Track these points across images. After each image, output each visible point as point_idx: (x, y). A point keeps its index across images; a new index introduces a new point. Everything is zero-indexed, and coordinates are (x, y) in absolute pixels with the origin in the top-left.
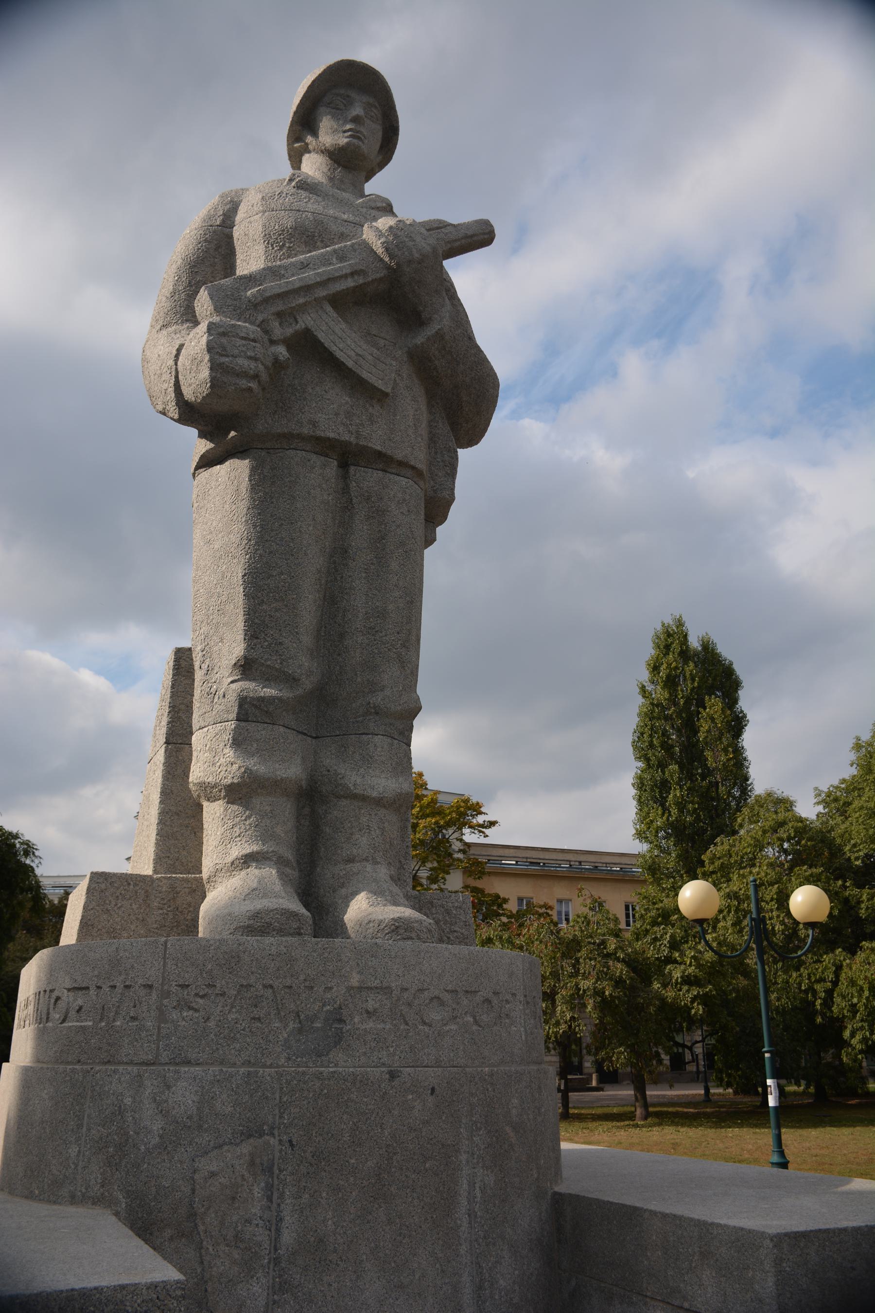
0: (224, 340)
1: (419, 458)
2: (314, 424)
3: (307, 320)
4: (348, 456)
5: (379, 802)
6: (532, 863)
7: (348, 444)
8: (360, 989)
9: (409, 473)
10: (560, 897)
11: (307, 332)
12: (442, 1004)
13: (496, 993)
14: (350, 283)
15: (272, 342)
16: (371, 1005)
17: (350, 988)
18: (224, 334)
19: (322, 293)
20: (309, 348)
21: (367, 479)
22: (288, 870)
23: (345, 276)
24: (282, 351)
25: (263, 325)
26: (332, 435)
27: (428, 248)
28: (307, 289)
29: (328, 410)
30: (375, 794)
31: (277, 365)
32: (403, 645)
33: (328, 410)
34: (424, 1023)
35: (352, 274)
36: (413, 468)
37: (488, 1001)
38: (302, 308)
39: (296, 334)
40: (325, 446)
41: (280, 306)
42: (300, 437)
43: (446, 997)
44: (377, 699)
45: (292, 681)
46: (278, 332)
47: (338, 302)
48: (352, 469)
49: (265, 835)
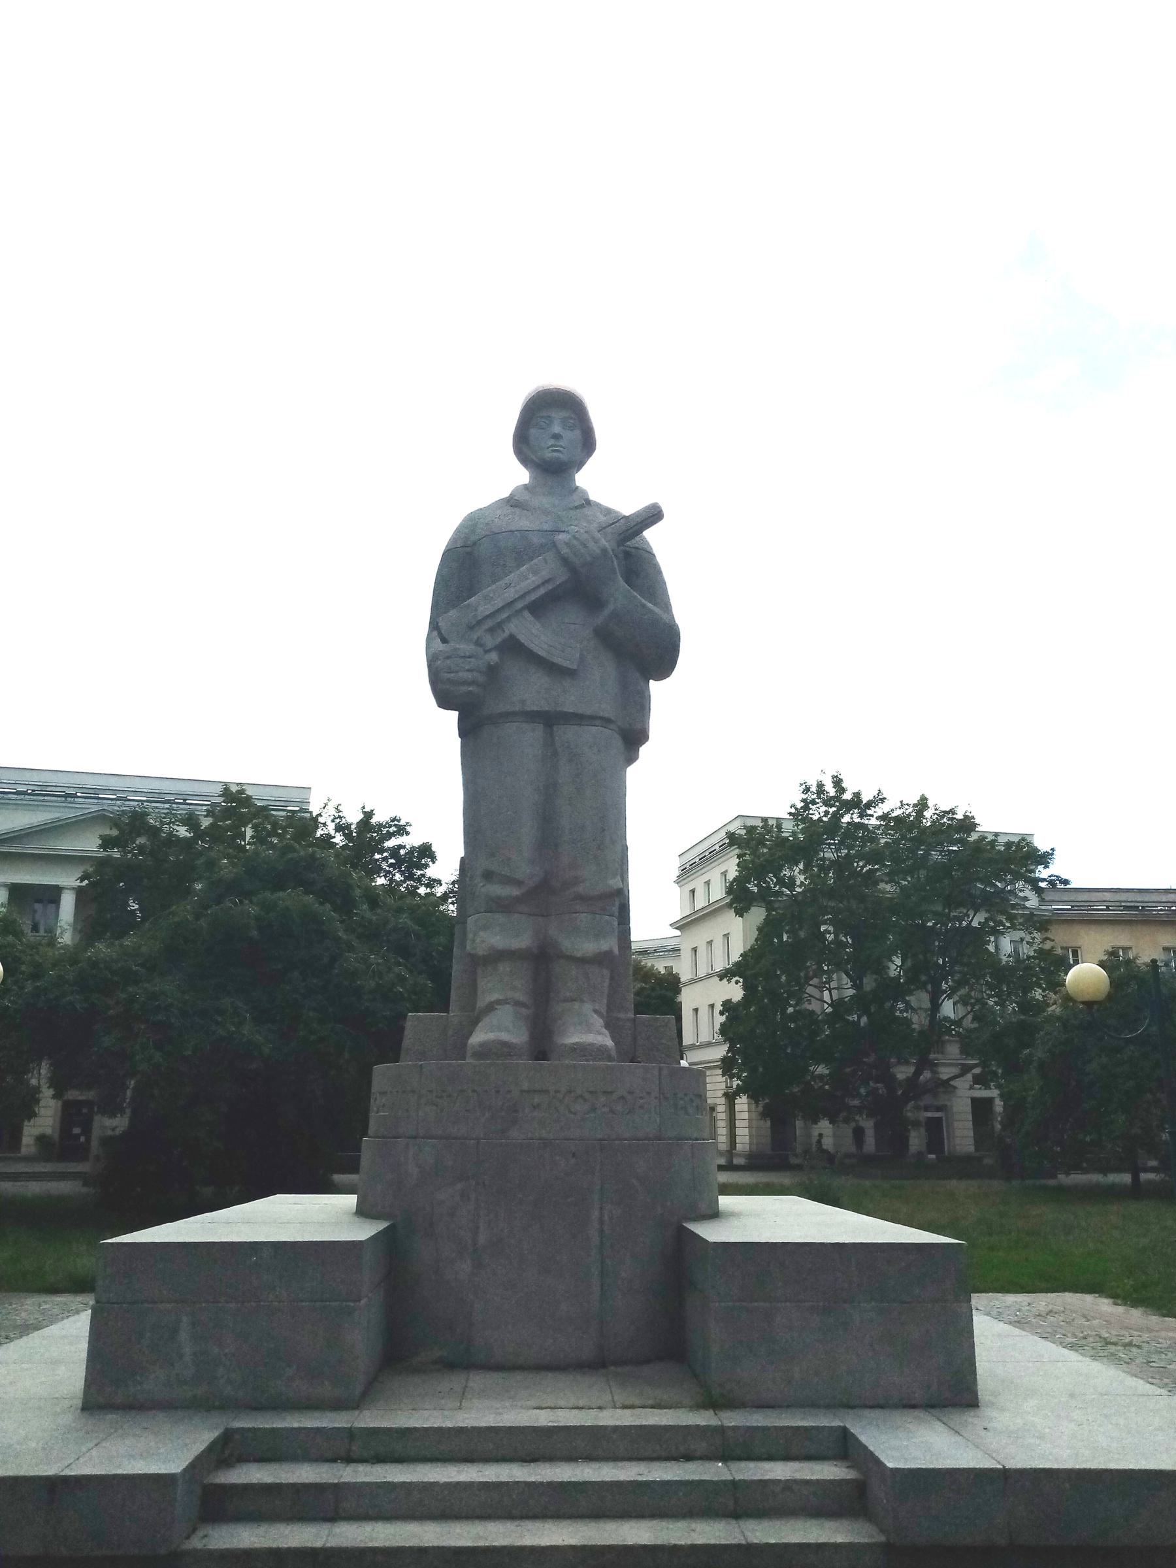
0: (448, 662)
1: (607, 708)
2: (523, 702)
3: (512, 628)
4: (550, 720)
5: (583, 961)
6: (1127, 908)
7: (547, 712)
8: (528, 1092)
9: (598, 722)
10: (1167, 945)
11: (512, 637)
12: (585, 1100)
13: (630, 1093)
14: (542, 591)
15: (487, 652)
16: (536, 1100)
17: (522, 1091)
18: (448, 658)
19: (519, 605)
20: (513, 648)
21: (567, 734)
22: (524, 1011)
23: (538, 587)
24: (494, 657)
25: (478, 643)
26: (535, 709)
27: (598, 551)
28: (510, 604)
29: (530, 690)
30: (579, 955)
31: (492, 671)
32: (599, 848)
33: (530, 690)
34: (571, 1112)
35: (543, 584)
36: (601, 718)
37: (623, 1098)
38: (508, 618)
39: (504, 641)
40: (533, 717)
41: (489, 623)
42: (514, 714)
43: (587, 1096)
44: (580, 889)
45: (519, 883)
46: (489, 641)
47: (538, 608)
48: (555, 728)
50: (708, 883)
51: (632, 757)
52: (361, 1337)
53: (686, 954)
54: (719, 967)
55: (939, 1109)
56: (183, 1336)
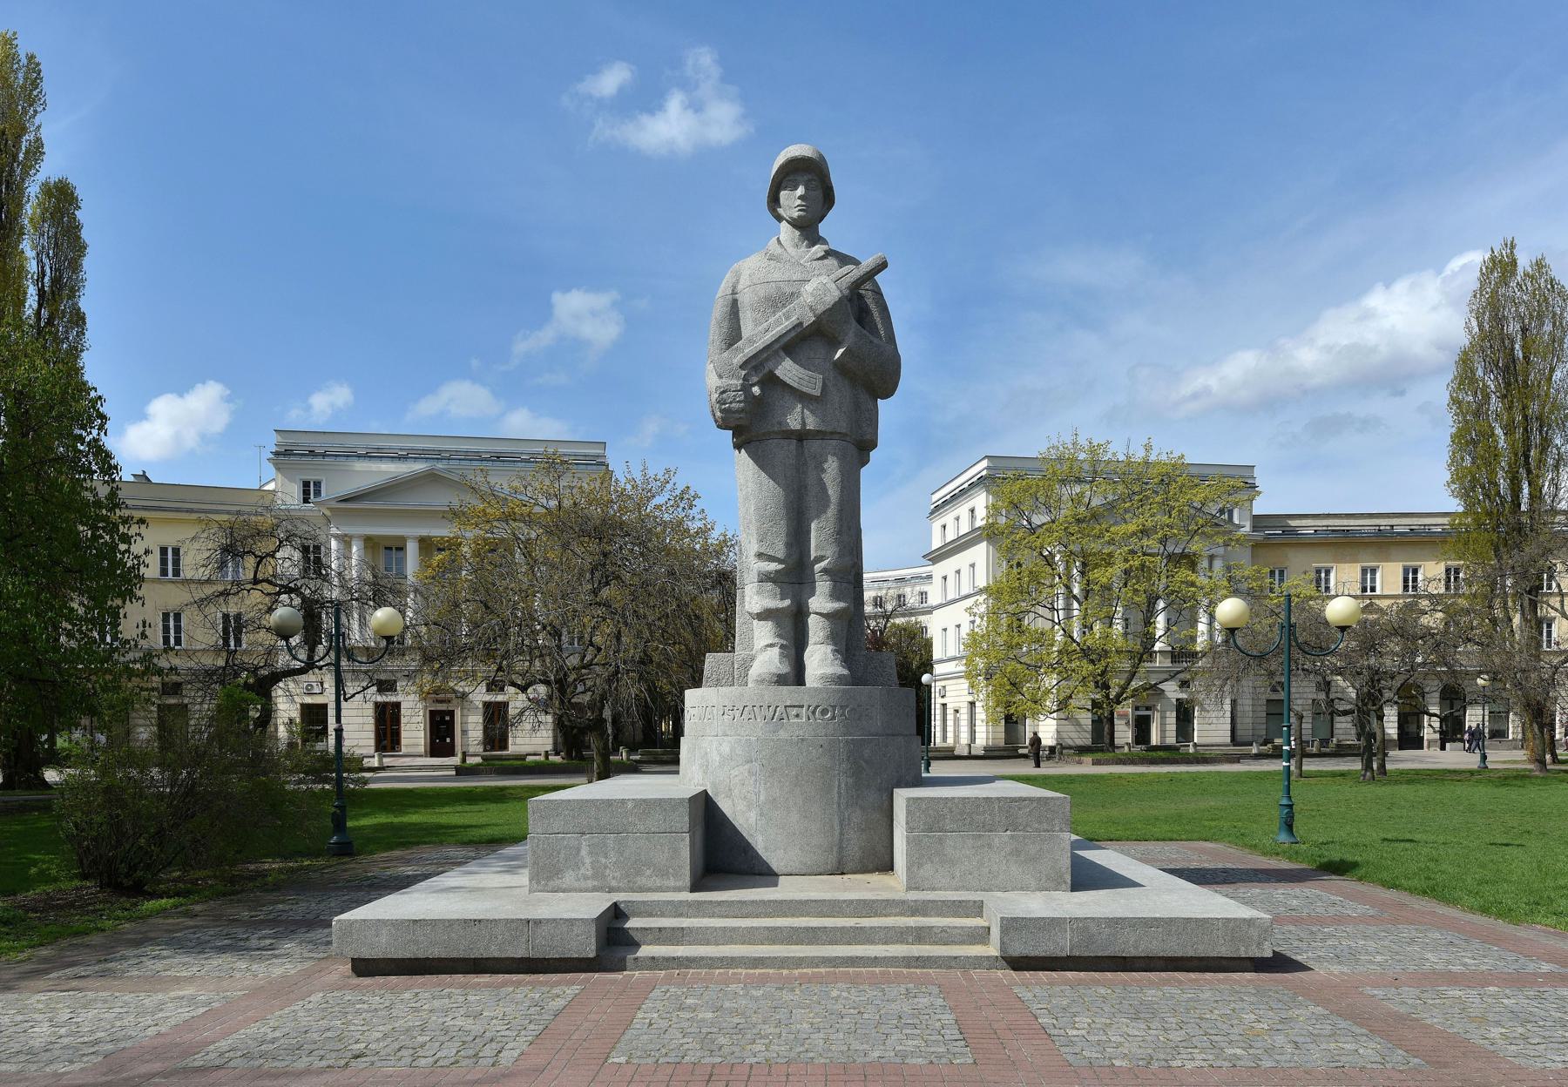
49: (788, 555)
50: (957, 519)
51: (864, 461)
52: (682, 852)
53: (937, 580)
54: (982, 582)
55: (1148, 709)
56: (584, 852)
